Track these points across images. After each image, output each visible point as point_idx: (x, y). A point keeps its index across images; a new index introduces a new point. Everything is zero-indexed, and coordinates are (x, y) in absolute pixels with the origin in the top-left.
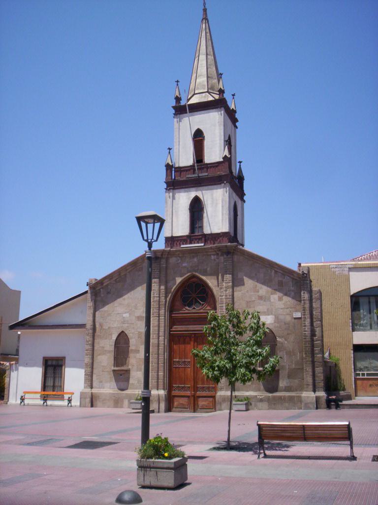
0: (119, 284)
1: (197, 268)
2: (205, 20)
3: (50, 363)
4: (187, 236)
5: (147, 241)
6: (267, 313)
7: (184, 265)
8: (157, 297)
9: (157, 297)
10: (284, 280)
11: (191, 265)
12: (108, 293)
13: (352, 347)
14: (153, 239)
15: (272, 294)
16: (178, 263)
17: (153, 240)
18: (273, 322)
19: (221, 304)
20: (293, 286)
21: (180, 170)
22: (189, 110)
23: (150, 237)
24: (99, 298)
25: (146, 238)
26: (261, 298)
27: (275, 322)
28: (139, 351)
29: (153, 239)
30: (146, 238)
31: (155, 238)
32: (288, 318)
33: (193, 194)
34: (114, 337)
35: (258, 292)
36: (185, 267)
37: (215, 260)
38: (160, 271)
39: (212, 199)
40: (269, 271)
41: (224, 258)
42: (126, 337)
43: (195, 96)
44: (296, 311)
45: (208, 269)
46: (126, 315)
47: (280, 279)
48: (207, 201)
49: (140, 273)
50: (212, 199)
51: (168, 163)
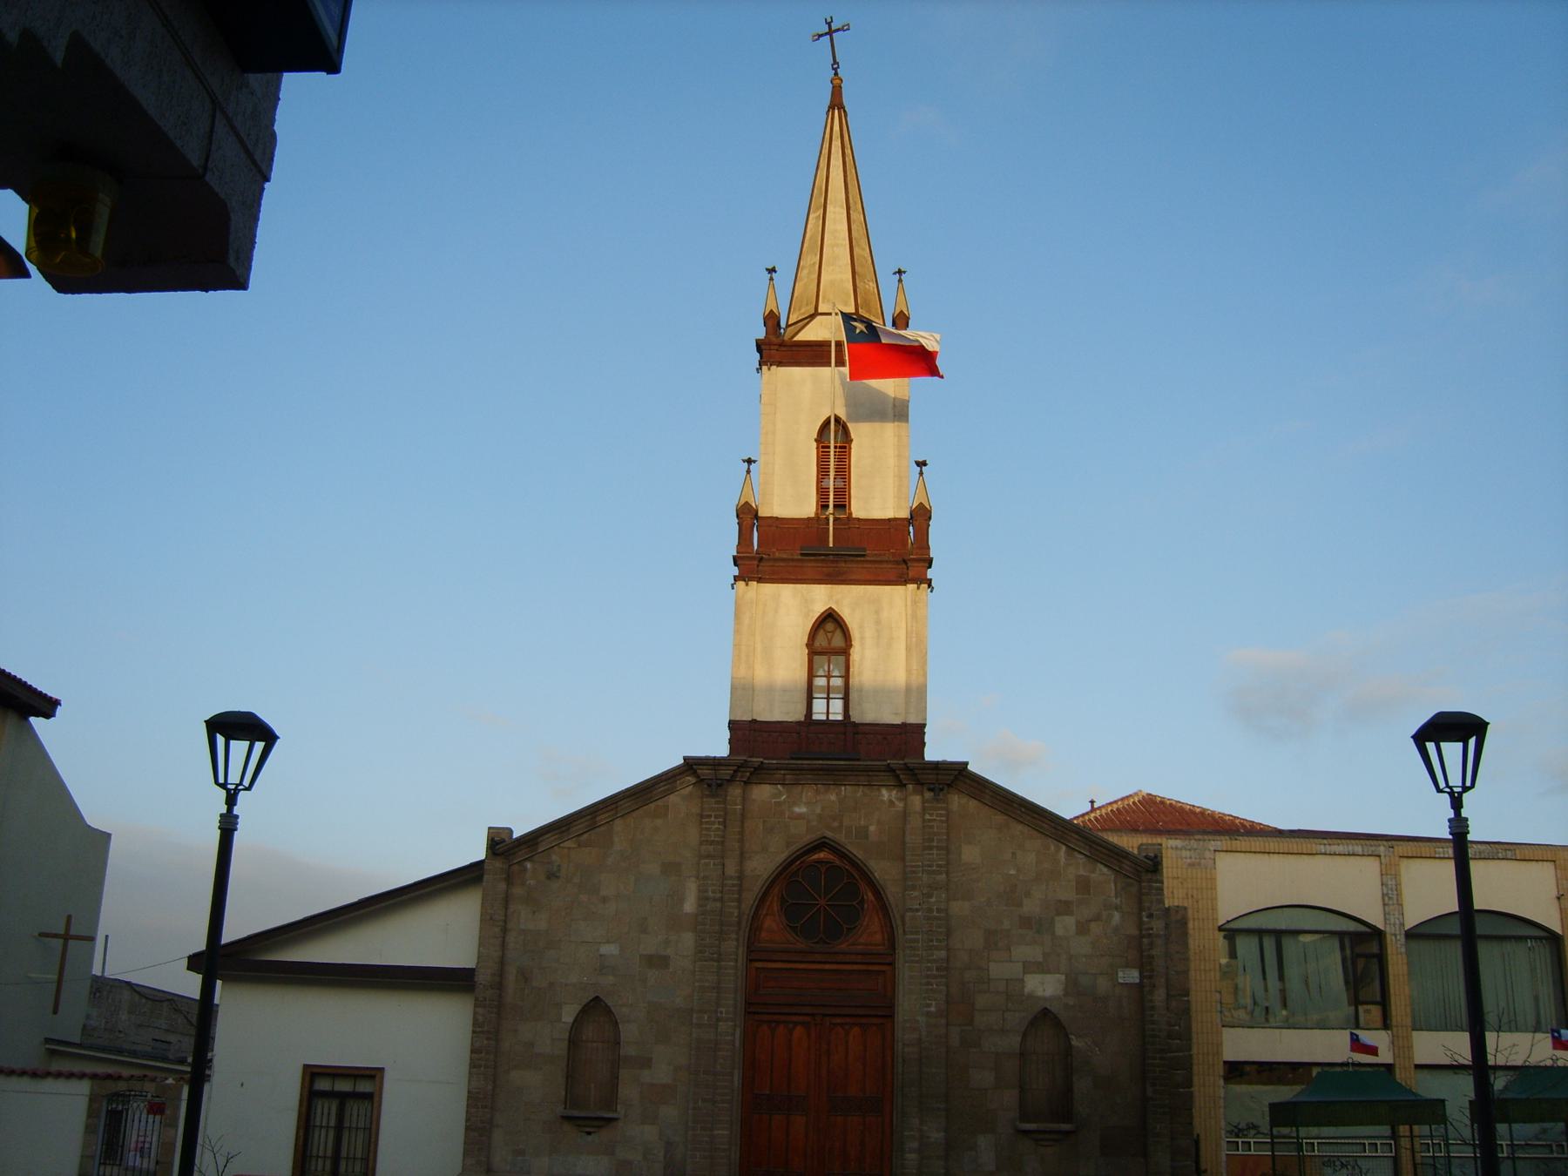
0: (583, 849)
1: (836, 824)
2: (838, 109)
3: (323, 1085)
4: (799, 723)
5: (224, 786)
6: (1041, 968)
7: (797, 810)
8: (715, 900)
9: (715, 900)
10: (1093, 875)
11: (818, 811)
12: (552, 876)
13: (1220, 1070)
14: (241, 784)
15: (1058, 914)
16: (779, 804)
17: (240, 787)
18: (1060, 992)
19: (912, 933)
20: (1116, 898)
21: (778, 529)
22: (830, 346)
23: (234, 778)
24: (518, 891)
25: (221, 780)
26: (1026, 922)
27: (1066, 994)
28: (650, 1060)
29: (241, 784)
30: (221, 780)
31: (246, 783)
32: (1103, 984)
33: (820, 597)
34: (568, 1015)
35: (1020, 905)
36: (800, 817)
37: (891, 803)
38: (724, 824)
39: (878, 622)
40: (1053, 848)
41: (923, 802)
42: (1315, 1071)
43: (819, 318)
44: (1127, 966)
45: (872, 828)
46: (610, 949)
47: (1082, 872)
48: (861, 627)
49: (659, 822)
50: (878, 622)
51: (747, 503)
